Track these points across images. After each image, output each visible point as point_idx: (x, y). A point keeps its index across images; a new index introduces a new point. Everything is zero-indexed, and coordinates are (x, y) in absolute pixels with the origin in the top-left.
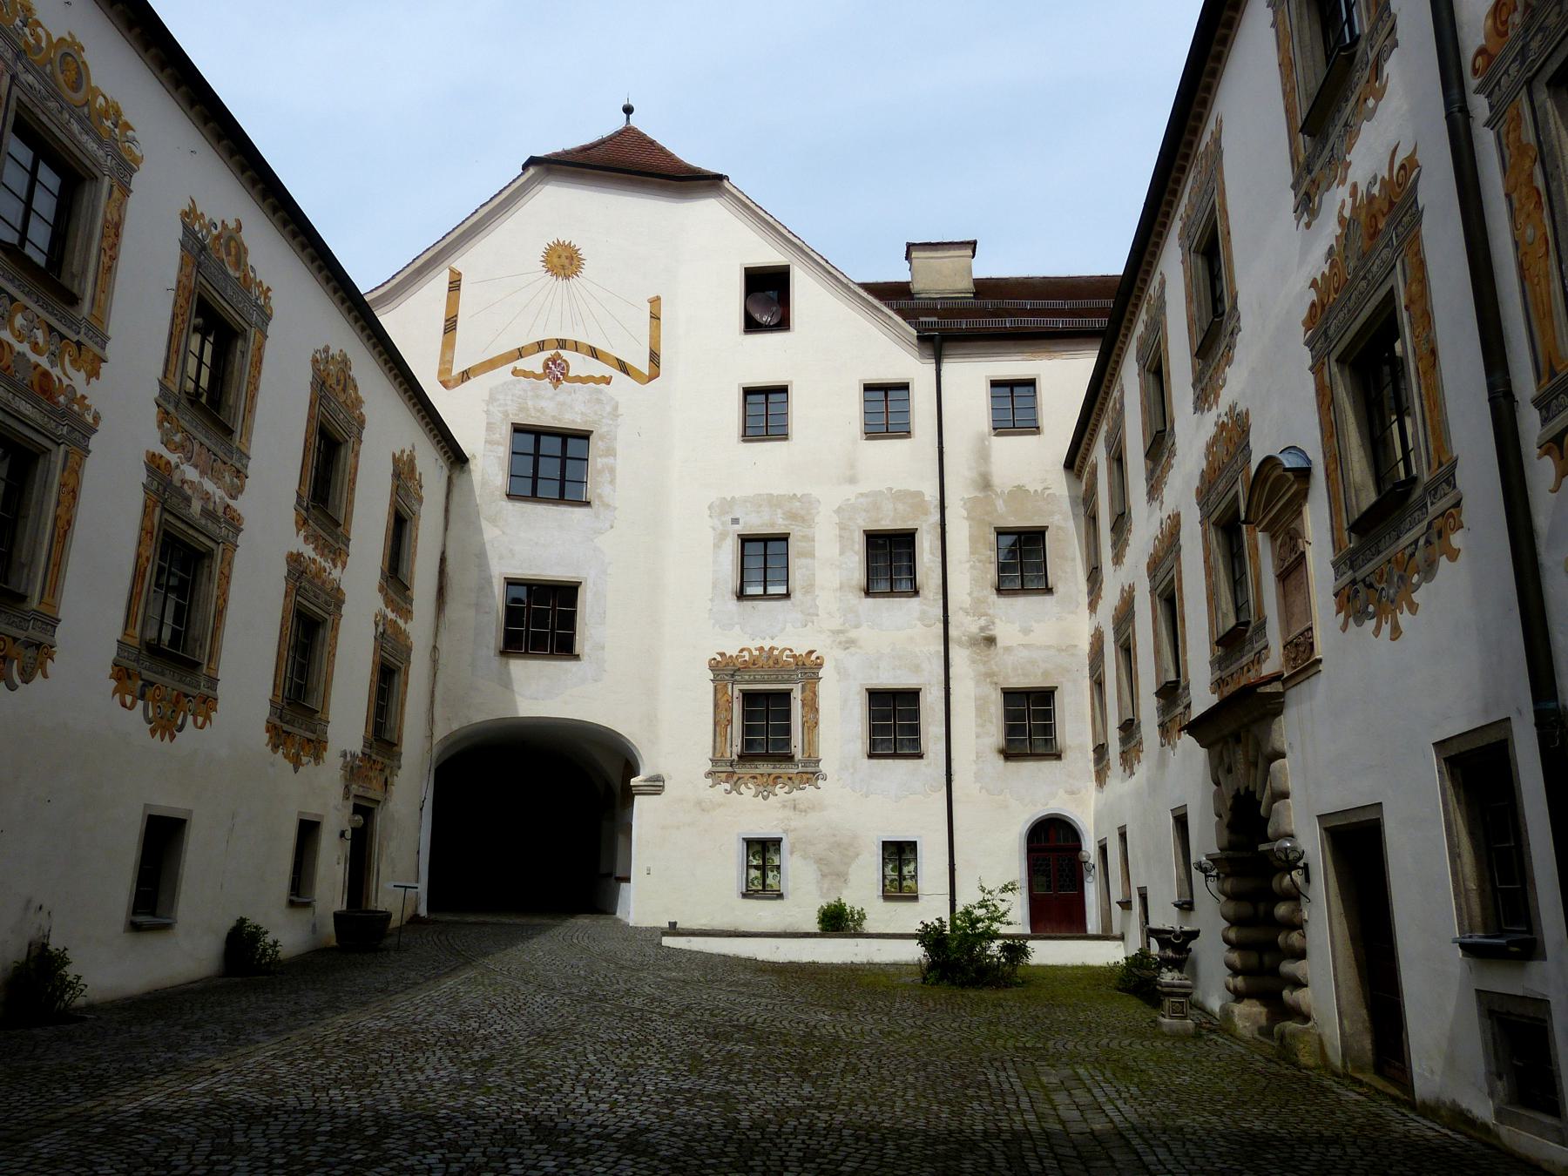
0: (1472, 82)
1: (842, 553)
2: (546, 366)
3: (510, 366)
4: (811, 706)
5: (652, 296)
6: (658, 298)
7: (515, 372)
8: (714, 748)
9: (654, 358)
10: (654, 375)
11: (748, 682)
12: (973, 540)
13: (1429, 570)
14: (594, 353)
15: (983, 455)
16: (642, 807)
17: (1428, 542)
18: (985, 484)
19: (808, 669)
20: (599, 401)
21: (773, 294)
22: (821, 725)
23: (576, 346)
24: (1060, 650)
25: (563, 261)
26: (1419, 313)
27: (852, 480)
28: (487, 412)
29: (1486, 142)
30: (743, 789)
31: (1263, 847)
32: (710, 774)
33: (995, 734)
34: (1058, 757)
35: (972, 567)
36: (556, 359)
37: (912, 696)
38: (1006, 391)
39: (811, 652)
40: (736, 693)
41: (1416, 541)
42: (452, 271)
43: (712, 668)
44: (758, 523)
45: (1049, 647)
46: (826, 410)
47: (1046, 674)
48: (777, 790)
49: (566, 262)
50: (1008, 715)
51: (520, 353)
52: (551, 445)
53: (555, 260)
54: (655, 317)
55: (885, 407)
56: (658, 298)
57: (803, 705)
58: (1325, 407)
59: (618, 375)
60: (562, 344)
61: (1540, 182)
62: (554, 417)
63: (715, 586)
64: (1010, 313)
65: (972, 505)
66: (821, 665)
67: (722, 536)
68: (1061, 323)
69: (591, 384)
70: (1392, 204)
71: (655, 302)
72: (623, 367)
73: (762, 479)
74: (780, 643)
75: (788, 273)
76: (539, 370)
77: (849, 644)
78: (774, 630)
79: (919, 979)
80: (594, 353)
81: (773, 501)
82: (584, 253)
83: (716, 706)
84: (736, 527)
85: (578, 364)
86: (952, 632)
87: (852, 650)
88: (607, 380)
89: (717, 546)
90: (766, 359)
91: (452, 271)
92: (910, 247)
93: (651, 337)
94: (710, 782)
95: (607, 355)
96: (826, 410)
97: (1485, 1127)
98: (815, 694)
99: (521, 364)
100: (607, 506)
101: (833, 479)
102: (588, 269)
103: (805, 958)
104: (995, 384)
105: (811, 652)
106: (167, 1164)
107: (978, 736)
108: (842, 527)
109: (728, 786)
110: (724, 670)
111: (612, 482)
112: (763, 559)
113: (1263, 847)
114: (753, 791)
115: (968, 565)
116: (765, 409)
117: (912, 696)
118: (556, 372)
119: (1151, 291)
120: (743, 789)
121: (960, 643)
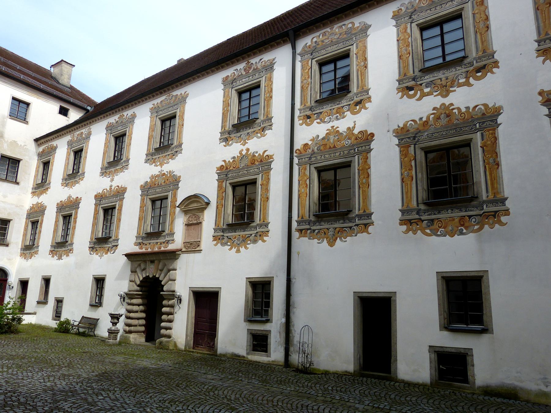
0: (295, 154)
13: (255, 241)
17: (255, 236)
24: (17, 206)
26: (265, 188)
29: (296, 168)
31: (161, 293)
34: (7, 245)
38: (17, 103)
41: (251, 235)
45: (12, 204)
47: (9, 214)
58: (221, 192)
61: (308, 182)
64: (24, 73)
68: (42, 86)
70: (261, 161)
97: (244, 357)
104: (14, 99)
106: (35, 408)
113: (161, 293)
119: (125, 114)
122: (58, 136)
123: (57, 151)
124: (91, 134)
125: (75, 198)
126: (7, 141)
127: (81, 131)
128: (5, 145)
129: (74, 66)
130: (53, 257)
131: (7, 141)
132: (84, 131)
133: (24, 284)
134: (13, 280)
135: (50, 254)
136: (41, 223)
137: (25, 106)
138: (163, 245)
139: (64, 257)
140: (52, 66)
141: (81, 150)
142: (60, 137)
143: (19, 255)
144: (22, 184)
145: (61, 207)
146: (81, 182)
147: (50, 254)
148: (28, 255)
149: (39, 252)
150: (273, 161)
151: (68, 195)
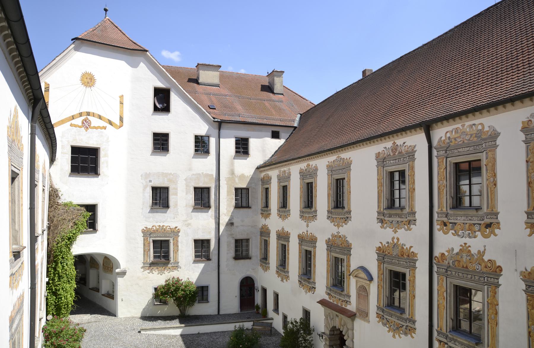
1: (186, 194)
2: (83, 123)
3: (69, 123)
4: (176, 245)
5: (121, 95)
6: (123, 96)
7: (71, 125)
9: (121, 119)
10: (121, 126)
11: (155, 237)
12: (228, 192)
14: (100, 117)
15: (232, 164)
18: (232, 173)
19: (175, 232)
22: (179, 251)
23: (94, 115)
25: (88, 80)
30: (154, 272)
32: (142, 267)
33: (232, 253)
35: (227, 200)
36: (86, 119)
37: (208, 189)
39: (176, 227)
40: (151, 241)
43: (143, 232)
44: (159, 183)
46: (182, 143)
48: (165, 272)
49: (89, 81)
51: (73, 117)
53: (85, 80)
54: (121, 103)
55: (201, 145)
56: (123, 96)
59: (108, 126)
60: (88, 114)
65: (229, 180)
66: (179, 232)
67: (145, 187)
71: (122, 97)
72: (111, 123)
74: (166, 224)
76: (80, 124)
77: (189, 225)
80: (100, 117)
82: (96, 77)
84: (150, 183)
87: (190, 227)
90: (162, 123)
93: (120, 111)
94: (142, 270)
95: (105, 118)
96: (182, 143)
98: (177, 241)
99: (74, 122)
101: (182, 169)
102: (97, 84)
105: (176, 227)
109: (149, 271)
110: (147, 233)
111: (107, 166)
112: (160, 197)
114: (157, 273)
116: (161, 142)
117: (208, 189)
118: (86, 124)
120: (154, 272)
128: (237, 180)
138: (344, 303)
144: (253, 207)
150: (417, 260)
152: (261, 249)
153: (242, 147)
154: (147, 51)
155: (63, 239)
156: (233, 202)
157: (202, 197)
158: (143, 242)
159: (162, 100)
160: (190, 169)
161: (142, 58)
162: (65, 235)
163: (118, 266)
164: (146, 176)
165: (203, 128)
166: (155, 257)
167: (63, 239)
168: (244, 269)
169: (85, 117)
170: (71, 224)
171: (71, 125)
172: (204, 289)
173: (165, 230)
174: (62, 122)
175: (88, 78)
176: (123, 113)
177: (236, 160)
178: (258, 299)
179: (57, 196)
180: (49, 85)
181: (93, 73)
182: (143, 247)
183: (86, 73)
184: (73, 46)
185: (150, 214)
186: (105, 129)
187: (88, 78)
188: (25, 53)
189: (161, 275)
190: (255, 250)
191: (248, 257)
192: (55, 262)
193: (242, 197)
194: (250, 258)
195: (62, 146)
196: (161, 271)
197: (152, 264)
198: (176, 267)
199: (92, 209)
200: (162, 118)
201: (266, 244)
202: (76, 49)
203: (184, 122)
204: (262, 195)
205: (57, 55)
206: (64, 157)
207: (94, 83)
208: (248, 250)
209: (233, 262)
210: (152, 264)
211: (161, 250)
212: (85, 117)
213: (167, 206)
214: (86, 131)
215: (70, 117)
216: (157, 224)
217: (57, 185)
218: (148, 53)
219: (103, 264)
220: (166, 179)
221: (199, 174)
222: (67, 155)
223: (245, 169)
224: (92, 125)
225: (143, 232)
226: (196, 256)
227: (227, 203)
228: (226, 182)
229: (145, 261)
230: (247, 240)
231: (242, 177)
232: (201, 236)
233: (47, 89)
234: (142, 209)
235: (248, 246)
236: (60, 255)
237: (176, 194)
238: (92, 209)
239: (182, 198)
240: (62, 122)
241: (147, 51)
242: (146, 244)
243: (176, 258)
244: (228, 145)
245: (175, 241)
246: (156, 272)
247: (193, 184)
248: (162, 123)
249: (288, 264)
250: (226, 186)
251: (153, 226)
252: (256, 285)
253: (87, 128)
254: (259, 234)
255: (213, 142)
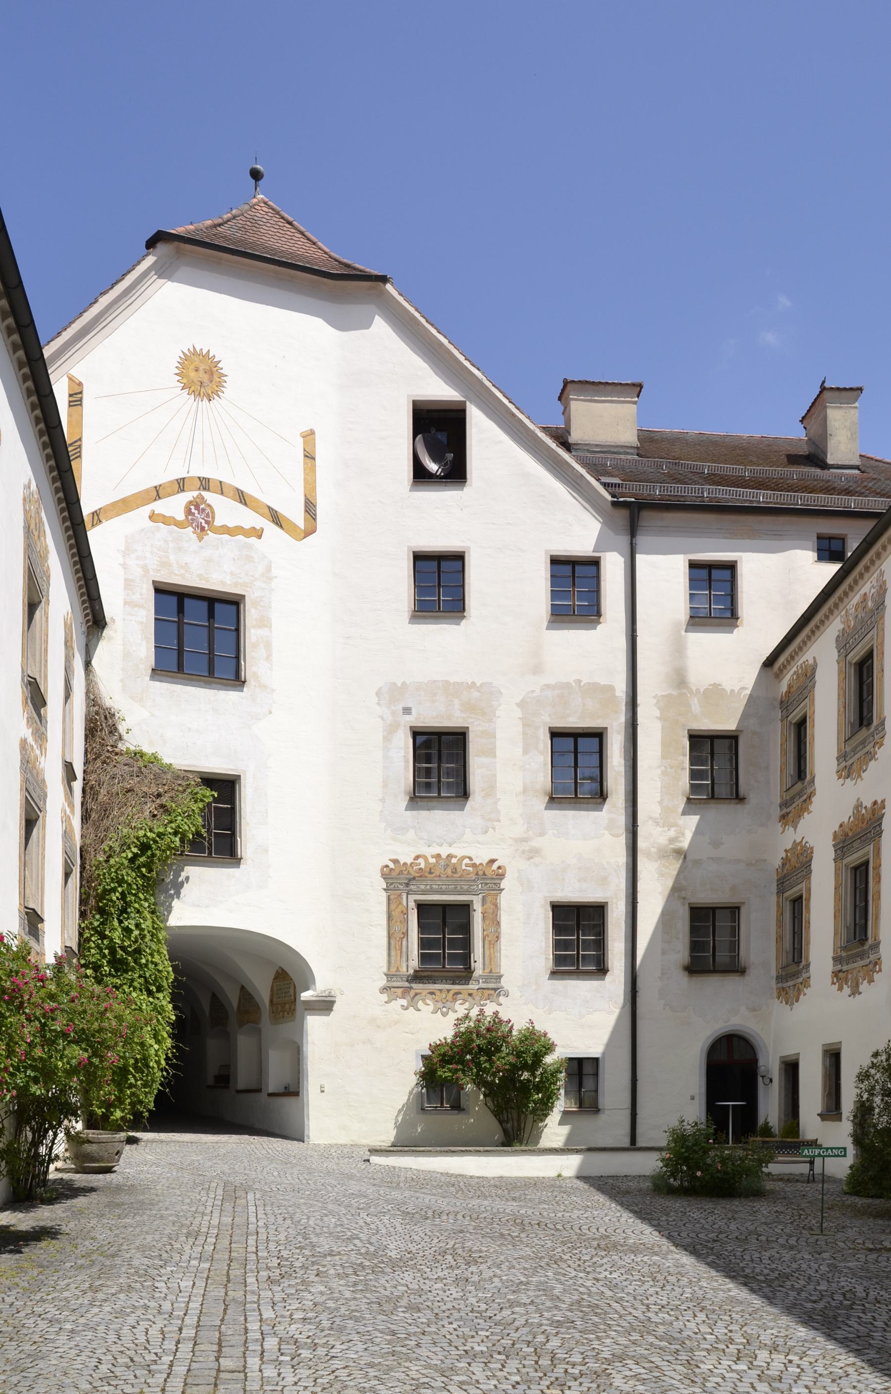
1: (526, 751)
2: (188, 512)
3: (146, 510)
4: (493, 919)
5: (305, 428)
6: (312, 432)
8: (389, 962)
9: (310, 508)
10: (310, 531)
11: (424, 892)
12: (666, 745)
14: (242, 498)
15: (679, 649)
16: (314, 1023)
18: (680, 679)
19: (490, 878)
20: (249, 559)
21: (442, 437)
22: (503, 940)
23: (221, 488)
25: (202, 376)
27: (537, 670)
28: (124, 566)
30: (420, 1004)
32: (385, 989)
35: (664, 773)
36: (197, 502)
37: (598, 735)
40: (412, 904)
42: (71, 379)
43: (385, 876)
46: (508, 585)
49: (205, 378)
50: (694, 930)
51: (158, 493)
52: (196, 612)
53: (193, 374)
54: (309, 456)
55: (574, 587)
56: (312, 432)
57: (484, 919)
59: (270, 528)
60: (205, 484)
62: (200, 576)
63: (385, 785)
65: (666, 704)
66: (501, 876)
67: (390, 731)
68: (762, 497)
69: (240, 537)
71: (309, 436)
72: (276, 518)
73: (443, 667)
75: (463, 411)
76: (181, 516)
77: (534, 853)
78: (450, 837)
79: (648, 1184)
80: (242, 498)
81: (451, 689)
82: (226, 367)
83: (390, 917)
85: (226, 511)
86: (641, 844)
87: (537, 860)
88: (258, 533)
89: (387, 739)
90: (439, 519)
91: (71, 379)
92: (566, 383)
94: (384, 997)
95: (256, 500)
96: (508, 585)
98: (496, 906)
100: (264, 687)
101: (511, 667)
102: (229, 391)
103: (787, 1172)
105: (493, 861)
107: (664, 952)
108: (527, 724)
109: (404, 1002)
110: (397, 878)
111: (269, 657)
112: (440, 761)
114: (431, 1008)
115: (659, 771)
116: (439, 583)
117: (598, 735)
118: (199, 519)
120: (420, 1004)
121: (648, 855)
122: (813, 632)
123: (817, 678)
124: (886, 590)
125: (869, 805)
126: (698, 690)
127: (862, 592)
128: (695, 705)
129: (860, 389)
130: (840, 989)
131: (698, 690)
132: (867, 587)
133: (791, 1068)
134: (770, 1063)
135: (833, 983)
136: (808, 900)
137: (727, 574)
139: (864, 986)
140: (803, 418)
141: (869, 655)
142: (817, 633)
143: (775, 994)
144: (753, 799)
145: (844, 843)
146: (880, 753)
147: (833, 983)
148: (792, 993)
149: (812, 982)
151: (854, 803)
152: (780, 938)
153: (715, 594)
154: (384, 279)
155: (125, 846)
156: (685, 780)
157: (579, 762)
158: (384, 907)
159: (440, 439)
160: (537, 670)
161: (372, 308)
162: (133, 833)
163: (308, 980)
164: (394, 693)
165: (580, 530)
166: (424, 958)
167: (125, 846)
168: (722, 1007)
169: (195, 494)
170: (150, 807)
171: (153, 517)
172: (588, 1069)
173: (455, 871)
174: (124, 505)
175: (202, 367)
176: (314, 489)
177: (690, 634)
178: (770, 1108)
179: (113, 730)
180: (80, 384)
181: (217, 352)
182: (384, 922)
183: (195, 353)
184: (150, 260)
185: (409, 812)
186: (260, 537)
187: (202, 367)
188: (89, 576)
189: (444, 1015)
190: (759, 940)
191: (736, 968)
192: (102, 911)
193: (714, 757)
194: (741, 971)
195: (126, 580)
196: (445, 1001)
197: (418, 977)
198: (495, 991)
199: (225, 788)
200: (440, 499)
201: (797, 908)
202: (163, 271)
203: (518, 510)
204: (784, 752)
205: (98, 284)
206: (131, 625)
207: (220, 385)
208: (734, 946)
209: (683, 979)
210: (418, 977)
211: (443, 934)
212: (195, 494)
213: (464, 794)
214: (200, 539)
215: (147, 491)
216: (429, 852)
217: (113, 695)
218: (389, 287)
219: (271, 1001)
220: (456, 702)
221: (567, 685)
222: (143, 612)
223: (726, 668)
224: (218, 522)
225: (387, 874)
226: (559, 960)
227: (663, 774)
228: (657, 713)
229: (393, 970)
230: (734, 911)
231: (714, 693)
232: (577, 892)
233: (76, 399)
234: (383, 800)
235: (735, 931)
236: (114, 890)
237: (491, 752)
238: (225, 788)
239: (510, 763)
240: (124, 505)
241: (384, 279)
242: (396, 914)
243: (491, 959)
244: (664, 574)
245: (488, 905)
246: (426, 1007)
247: (548, 720)
248: (439, 519)
249: (877, 918)
250: (658, 725)
251: (417, 858)
252: (761, 1063)
253: (203, 529)
254: (774, 888)
255: (613, 568)
